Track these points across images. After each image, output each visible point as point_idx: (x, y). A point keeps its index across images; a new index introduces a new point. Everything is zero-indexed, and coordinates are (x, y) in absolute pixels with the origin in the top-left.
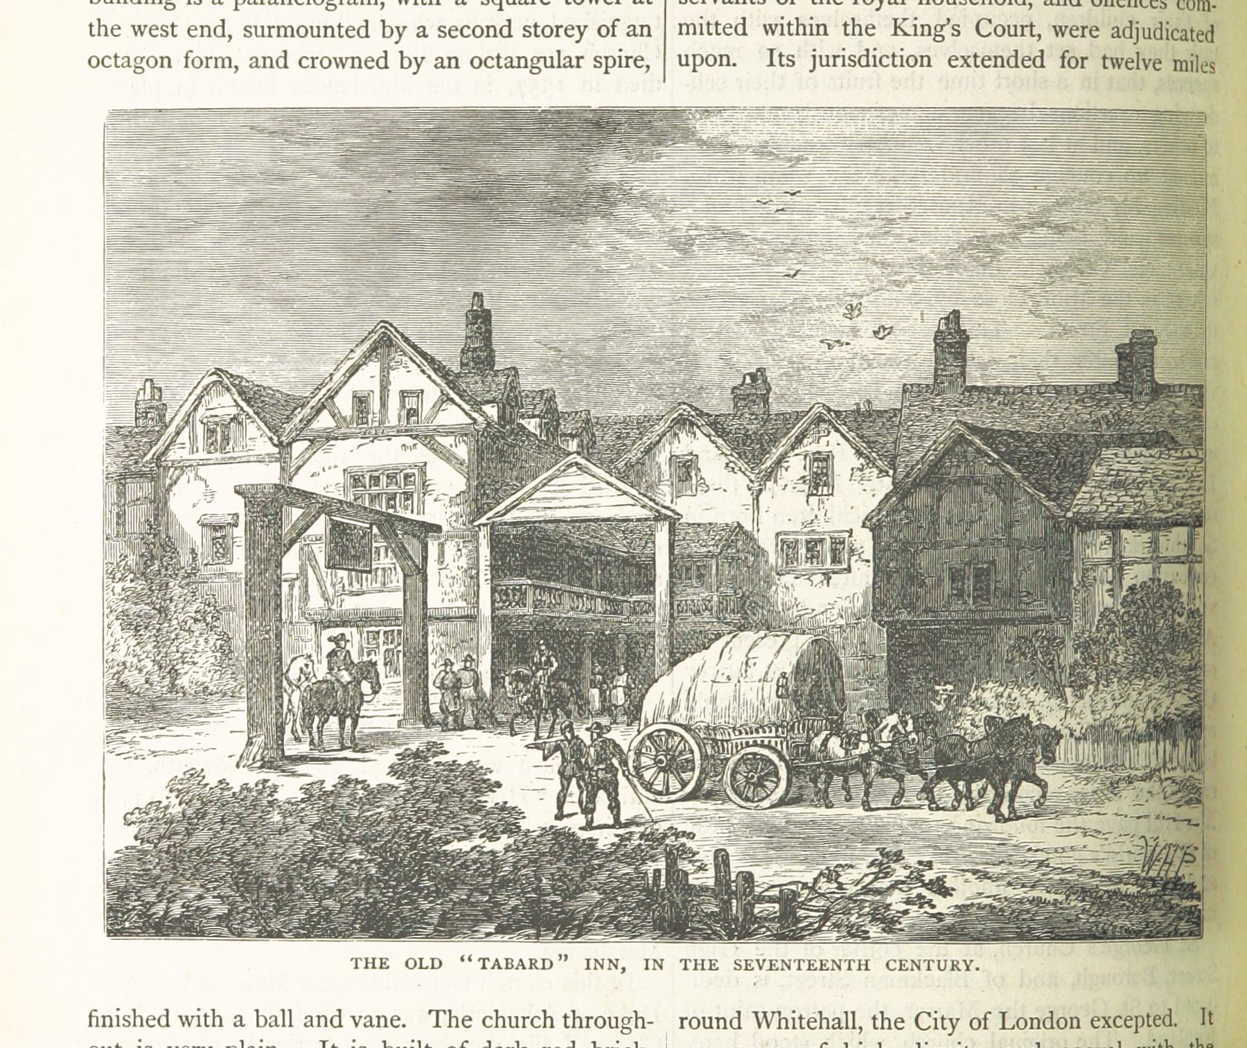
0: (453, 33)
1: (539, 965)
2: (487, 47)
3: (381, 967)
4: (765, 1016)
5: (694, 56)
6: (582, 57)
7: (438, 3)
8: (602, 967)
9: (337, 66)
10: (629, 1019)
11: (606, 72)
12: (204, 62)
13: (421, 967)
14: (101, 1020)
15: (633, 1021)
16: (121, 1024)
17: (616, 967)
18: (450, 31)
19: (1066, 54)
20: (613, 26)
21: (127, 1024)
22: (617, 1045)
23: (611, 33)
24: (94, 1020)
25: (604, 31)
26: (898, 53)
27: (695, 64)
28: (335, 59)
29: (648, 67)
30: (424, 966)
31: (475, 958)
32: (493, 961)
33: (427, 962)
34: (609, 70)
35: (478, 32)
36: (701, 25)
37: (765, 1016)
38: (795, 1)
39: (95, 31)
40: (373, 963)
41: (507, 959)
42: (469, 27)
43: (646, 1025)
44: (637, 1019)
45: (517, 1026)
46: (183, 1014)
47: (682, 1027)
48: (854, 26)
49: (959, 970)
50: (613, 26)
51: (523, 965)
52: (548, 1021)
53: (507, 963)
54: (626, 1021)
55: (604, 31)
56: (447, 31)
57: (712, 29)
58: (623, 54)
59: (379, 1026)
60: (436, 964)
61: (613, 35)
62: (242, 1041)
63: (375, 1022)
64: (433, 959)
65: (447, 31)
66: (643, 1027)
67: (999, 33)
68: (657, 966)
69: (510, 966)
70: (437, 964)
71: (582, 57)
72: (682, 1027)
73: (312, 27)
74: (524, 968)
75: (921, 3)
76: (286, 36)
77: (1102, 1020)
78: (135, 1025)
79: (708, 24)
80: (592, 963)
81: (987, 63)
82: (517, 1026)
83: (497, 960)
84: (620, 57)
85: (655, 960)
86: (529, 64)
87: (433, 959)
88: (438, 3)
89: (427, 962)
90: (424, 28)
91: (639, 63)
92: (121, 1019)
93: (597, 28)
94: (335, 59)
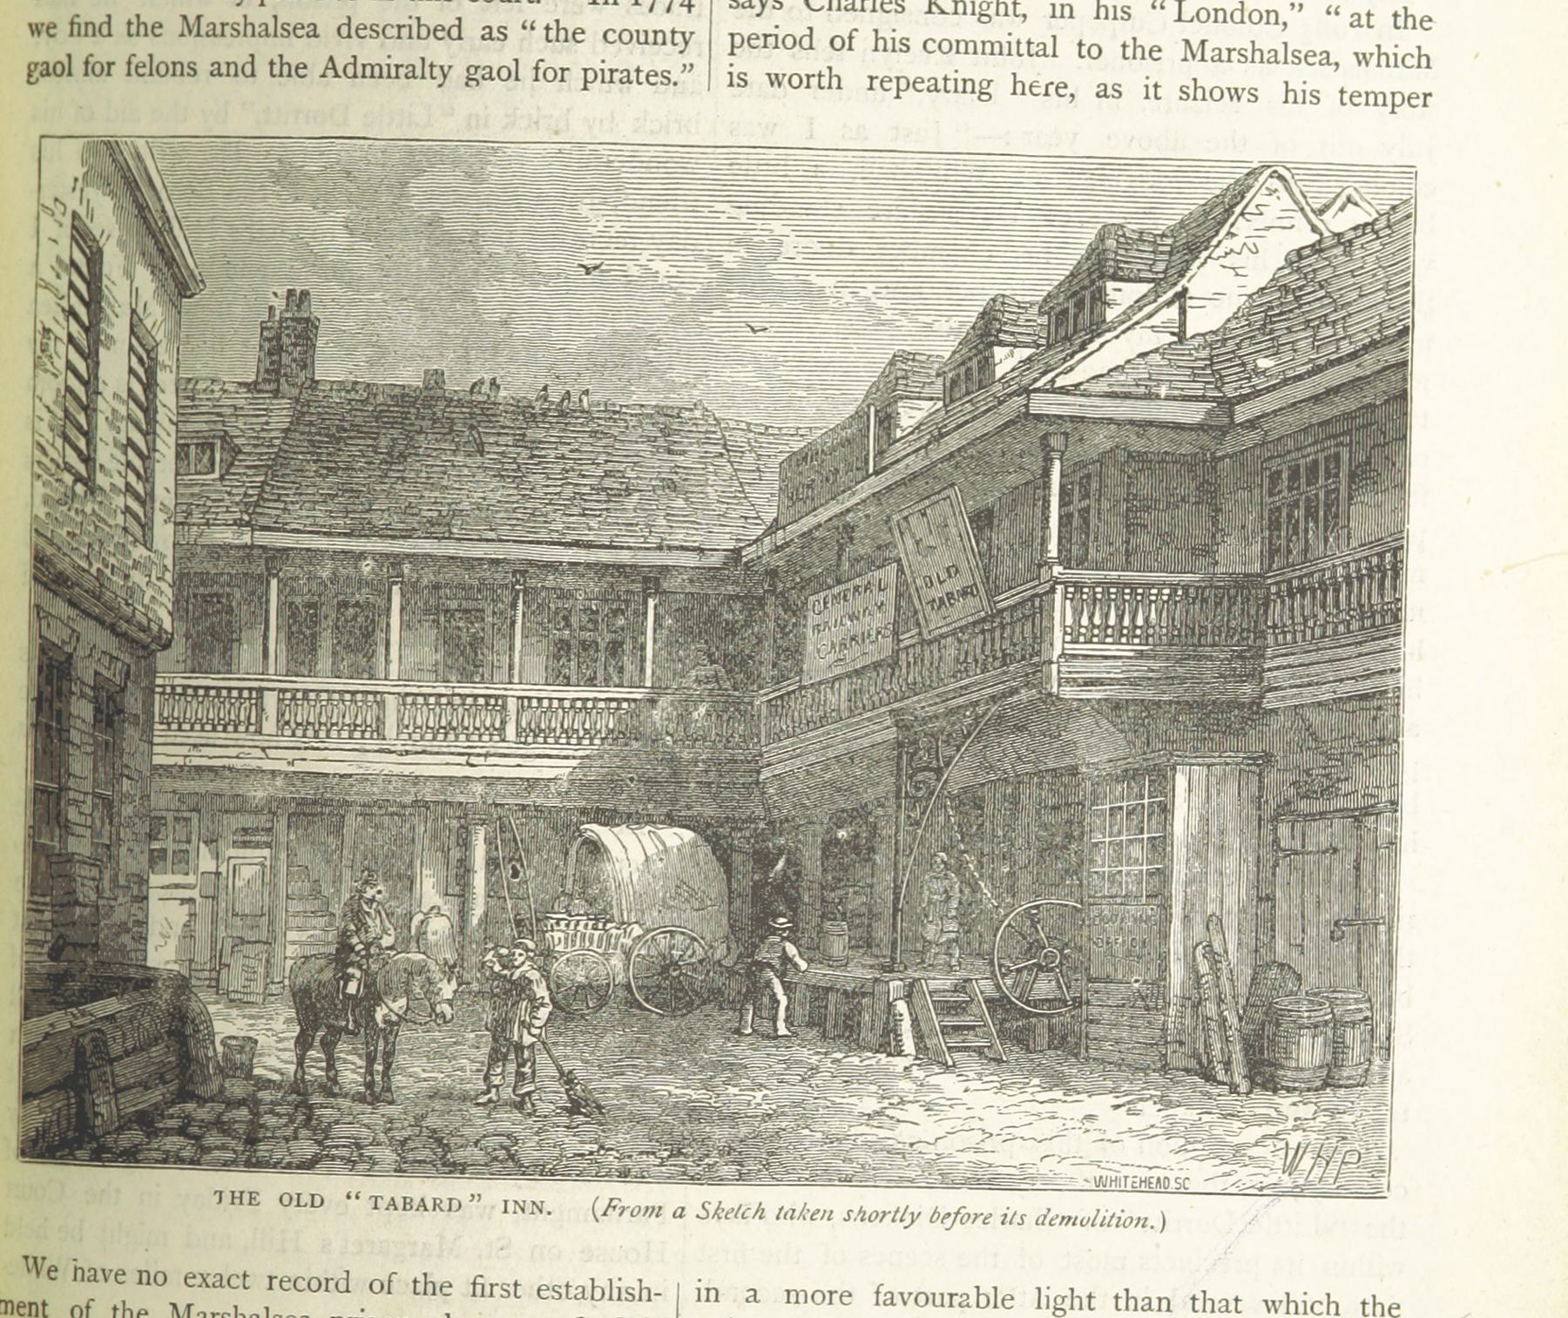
0: (440, 34)
1: (445, 1205)
2: (783, 61)
3: (250, 1204)
4: (35, 1263)
5: (1393, 94)
6: (1430, 95)
7: (615, 3)
8: (523, 1210)
9: (1232, 98)
10: (1063, 1298)
11: (898, 97)
12: (1208, 95)
13: (298, 1205)
14: (488, 1289)
15: (1068, 1301)
16: (623, 1297)
17: (541, 1211)
18: (295, 28)
19: (541, 64)
20: (851, 38)
21: (630, 1298)
22: (361, 1315)
23: (847, 46)
24: (479, 1288)
25: (838, 43)
26: (952, 75)
27: (1393, 105)
28: (1229, 89)
29: (1072, 95)
30: (302, 1203)
31: (364, 1196)
32: (387, 1200)
33: (306, 1199)
34: (901, 94)
35: (945, 46)
36: (1009, 43)
37: (35, 1263)
38: (640, 1)
39: (1129, 52)
40: (241, 1198)
41: (405, 1198)
42: (614, 31)
43: (653, 1297)
44: (1288, 1303)
45: (942, 1305)
46: (1270, 1298)
47: (271, 1288)
48: (558, 30)
49: (441, 1210)
50: (851, 38)
51: (425, 1206)
52: (1333, 1307)
53: (405, 1203)
54: (1059, 1300)
55: (838, 43)
56: (291, 29)
57: (1024, 48)
58: (606, 67)
59: (1160, 1310)
60: (316, 1202)
61: (850, 49)
62: (267, 1309)
63: (1155, 1305)
64: (313, 1196)
65: (291, 29)
66: (649, 1300)
67: (946, 50)
68: (518, 1209)
69: (408, 1207)
70: (317, 1201)
71: (1430, 95)
72: (271, 1288)
73: (638, 31)
74: (426, 1210)
75: (594, 3)
76: (966, 53)
77: (199, 1277)
78: (640, 1299)
79: (1019, 43)
80: (511, 1206)
81: (1356, 100)
82: (942, 1305)
83: (393, 1199)
84: (602, 70)
85: (516, 1202)
86: (977, 89)
87: (313, 1196)
88: (615, 3)
89: (306, 1199)
90: (1328, 54)
91: (1061, 91)
92: (623, 1291)
93: (602, 34)
94: (1229, 89)
